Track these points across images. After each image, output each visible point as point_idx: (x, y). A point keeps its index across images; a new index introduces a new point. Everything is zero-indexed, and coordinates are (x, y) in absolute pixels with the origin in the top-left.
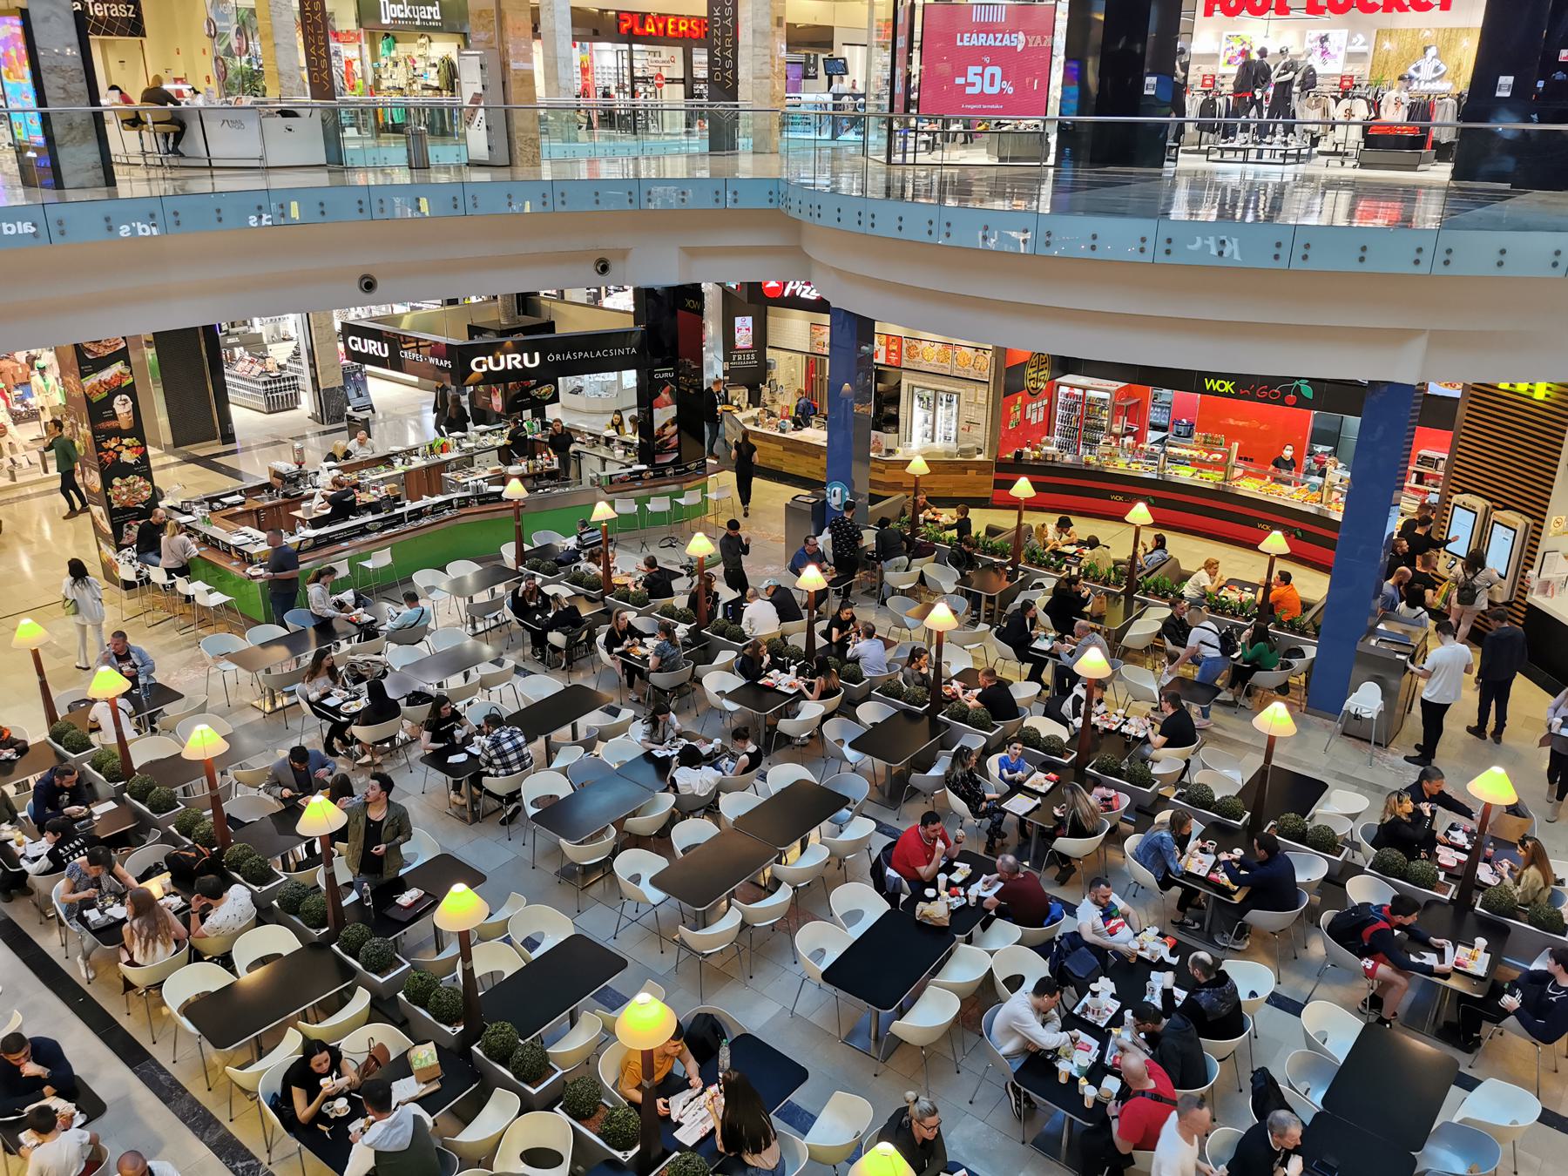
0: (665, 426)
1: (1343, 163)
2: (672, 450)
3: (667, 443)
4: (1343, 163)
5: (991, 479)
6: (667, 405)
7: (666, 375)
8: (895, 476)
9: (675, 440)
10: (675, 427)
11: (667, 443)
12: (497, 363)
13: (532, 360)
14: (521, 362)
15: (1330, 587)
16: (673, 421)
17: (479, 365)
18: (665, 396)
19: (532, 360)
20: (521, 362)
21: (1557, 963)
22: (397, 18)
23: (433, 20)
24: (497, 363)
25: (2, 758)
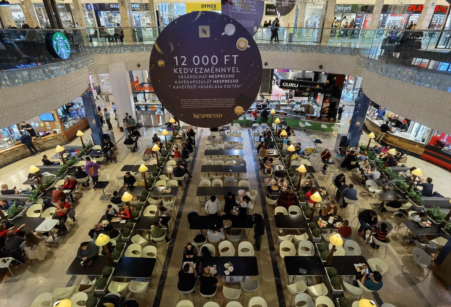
0: (326, 108)
1: (211, 157)
2: (326, 114)
3: (325, 112)
4: (211, 157)
5: (423, 150)
6: (327, 103)
7: (329, 96)
8: (391, 139)
9: (327, 112)
10: (328, 109)
11: (325, 112)
12: (288, 85)
13: (296, 86)
14: (294, 86)
15: (226, 203)
16: (328, 107)
17: (284, 84)
18: (327, 101)
19: (296, 86)
20: (294, 86)
22: (339, 10)
23: (349, 10)
24: (288, 85)
25: (328, 302)
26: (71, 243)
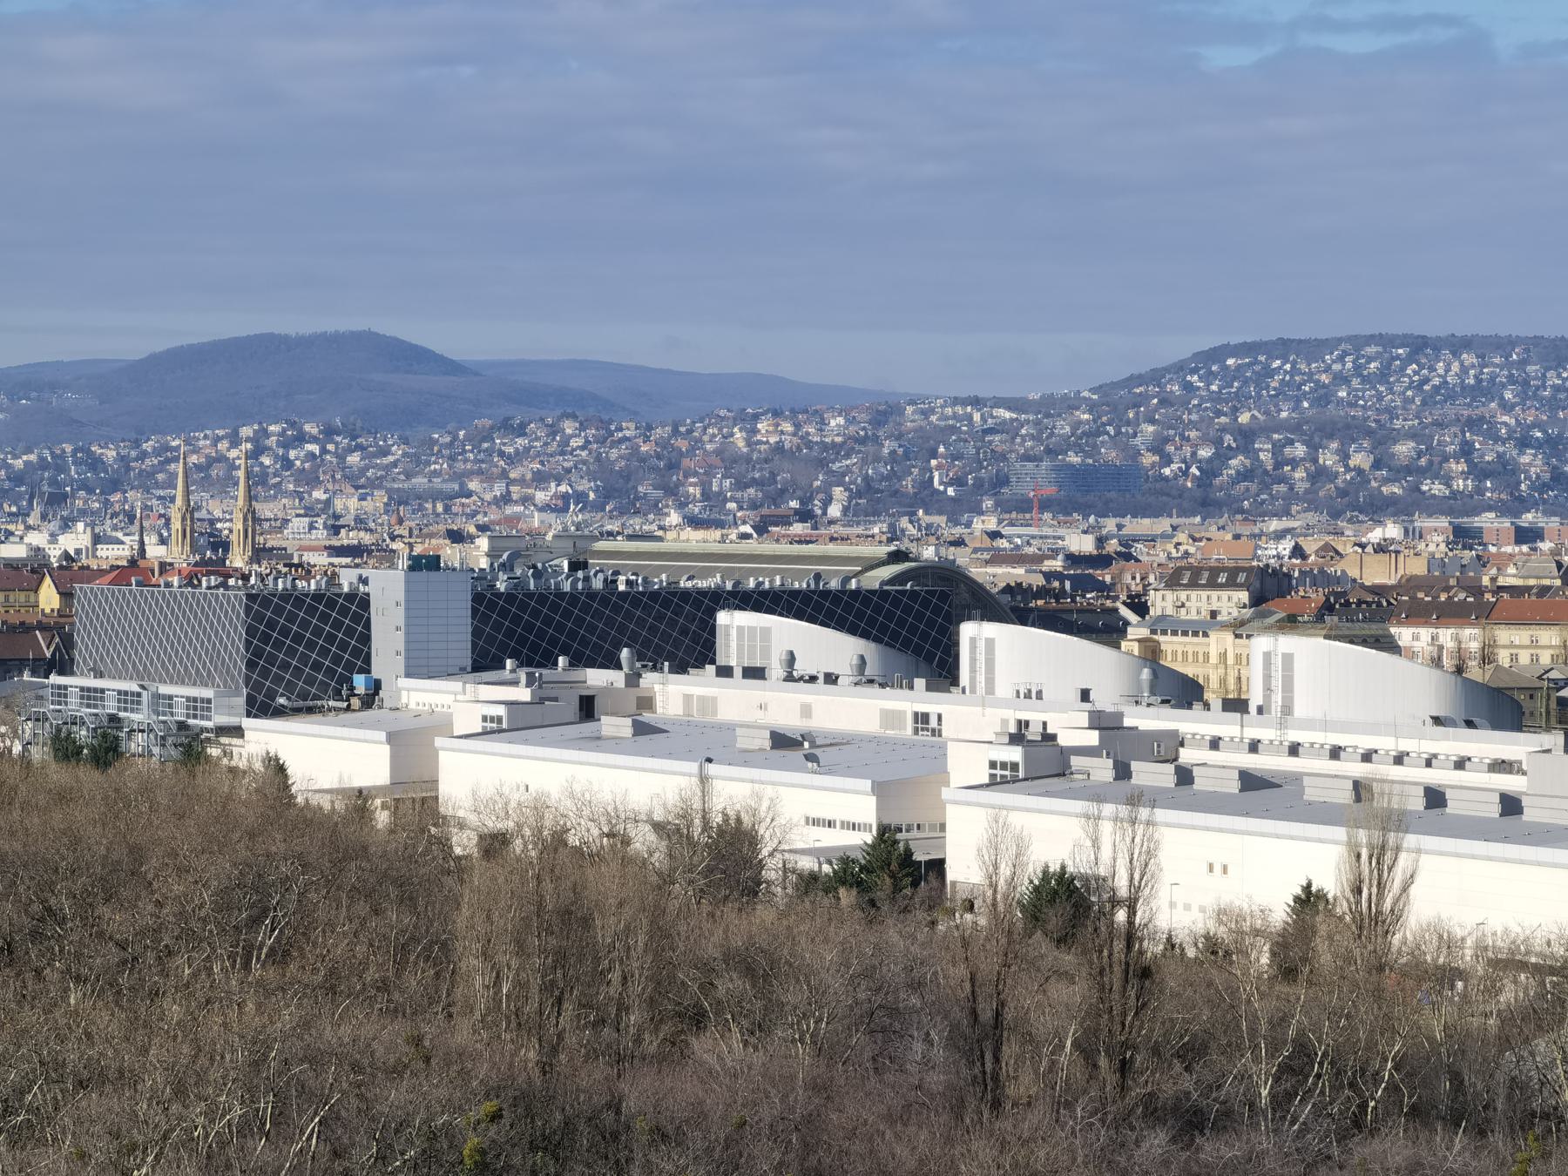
21: (278, 769)
26: (350, 778)
